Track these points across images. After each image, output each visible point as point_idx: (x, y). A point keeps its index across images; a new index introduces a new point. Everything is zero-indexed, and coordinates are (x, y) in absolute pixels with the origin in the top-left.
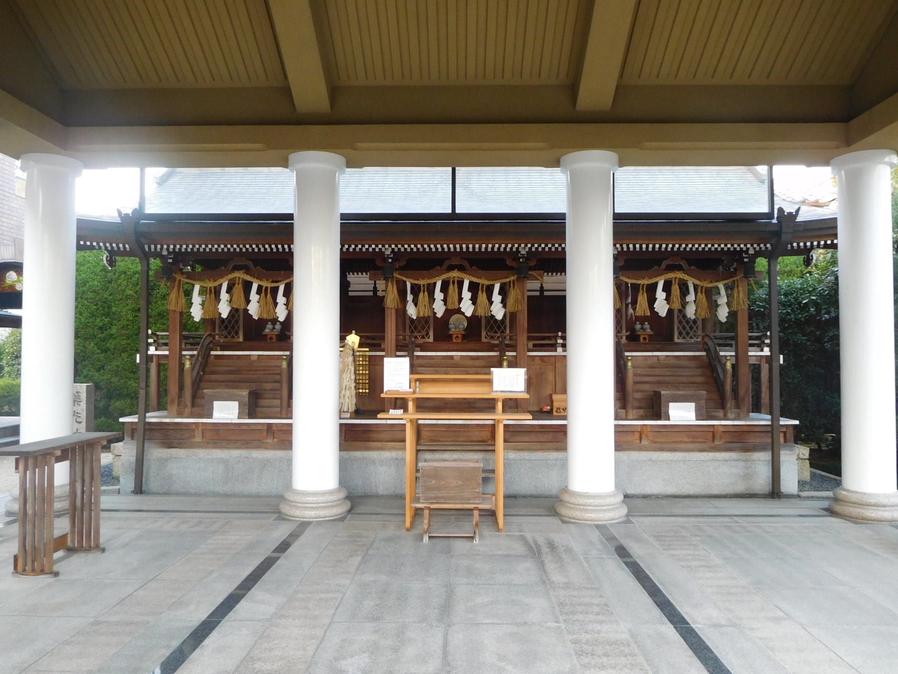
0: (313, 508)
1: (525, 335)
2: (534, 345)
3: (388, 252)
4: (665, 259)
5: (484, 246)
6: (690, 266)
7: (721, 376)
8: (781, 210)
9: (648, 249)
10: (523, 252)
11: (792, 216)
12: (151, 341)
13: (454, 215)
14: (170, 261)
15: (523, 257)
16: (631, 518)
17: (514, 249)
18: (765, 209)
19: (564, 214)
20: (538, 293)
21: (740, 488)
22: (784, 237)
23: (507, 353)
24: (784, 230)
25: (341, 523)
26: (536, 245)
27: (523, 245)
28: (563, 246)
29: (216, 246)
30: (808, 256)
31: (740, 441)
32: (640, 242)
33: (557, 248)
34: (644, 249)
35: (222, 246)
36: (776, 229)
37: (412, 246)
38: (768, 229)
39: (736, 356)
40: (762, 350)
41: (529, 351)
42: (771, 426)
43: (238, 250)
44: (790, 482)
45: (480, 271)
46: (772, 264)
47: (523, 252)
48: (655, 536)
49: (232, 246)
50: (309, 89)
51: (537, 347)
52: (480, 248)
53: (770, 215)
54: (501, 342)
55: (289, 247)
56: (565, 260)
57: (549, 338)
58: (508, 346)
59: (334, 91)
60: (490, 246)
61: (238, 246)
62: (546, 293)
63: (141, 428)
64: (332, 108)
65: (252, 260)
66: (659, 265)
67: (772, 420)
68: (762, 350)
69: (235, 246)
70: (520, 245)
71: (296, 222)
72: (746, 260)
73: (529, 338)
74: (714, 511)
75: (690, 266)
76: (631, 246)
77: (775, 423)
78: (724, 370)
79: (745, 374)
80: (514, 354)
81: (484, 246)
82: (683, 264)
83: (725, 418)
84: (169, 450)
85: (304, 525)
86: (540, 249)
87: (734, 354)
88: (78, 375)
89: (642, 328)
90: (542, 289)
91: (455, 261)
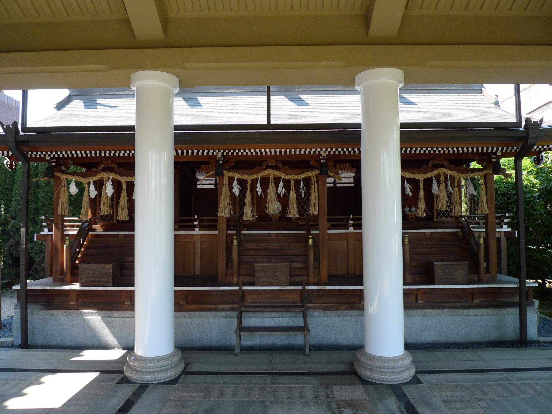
0: (150, 372)
1: (326, 218)
2: (332, 225)
3: (219, 156)
4: (432, 159)
5: (293, 150)
6: (451, 164)
7: (476, 249)
8: (528, 120)
9: (195, 152)
10: (324, 155)
11: (537, 124)
12: (44, 224)
13: (269, 126)
14: (54, 164)
15: (323, 159)
16: (421, 377)
17: (317, 153)
18: (513, 119)
19: (359, 124)
20: (332, 185)
21: (494, 336)
22: (530, 141)
23: (312, 232)
24: (531, 136)
25: (173, 386)
26: (424, 149)
27: (324, 150)
28: (133, 152)
29: (39, 153)
30: (538, 157)
31: (494, 300)
32: (406, 146)
33: (435, 151)
34: (480, 151)
35: (237, 151)
36: (524, 135)
37: (252, 151)
38: (518, 135)
39: (487, 232)
40: (502, 227)
41: (329, 229)
42: (519, 288)
43: (61, 156)
44: (532, 331)
45: (291, 170)
46: (518, 163)
47: (324, 155)
48: (444, 401)
49: (56, 153)
50: (145, 20)
51: (333, 227)
52: (290, 152)
53: (518, 124)
54: (306, 223)
55: (177, 153)
56: (360, 160)
57: (342, 220)
58: (312, 226)
59: (165, 21)
60: (298, 150)
61: (61, 153)
62: (338, 185)
63: (23, 295)
64: (165, 36)
65: (116, 163)
66: (427, 164)
67: (520, 283)
68: (502, 227)
69: (59, 153)
70: (321, 149)
71: (137, 133)
72: (494, 160)
73: (329, 220)
74: (483, 366)
75: (451, 164)
76: (470, 149)
77: (522, 287)
78: (478, 244)
79: (493, 244)
80: (317, 232)
81: (293, 150)
82: (445, 163)
83: (479, 282)
84: (50, 311)
85: (143, 387)
86: (427, 152)
87: (484, 230)
88: (134, 200)
89: (410, 211)
90: (335, 183)
91: (272, 162)
